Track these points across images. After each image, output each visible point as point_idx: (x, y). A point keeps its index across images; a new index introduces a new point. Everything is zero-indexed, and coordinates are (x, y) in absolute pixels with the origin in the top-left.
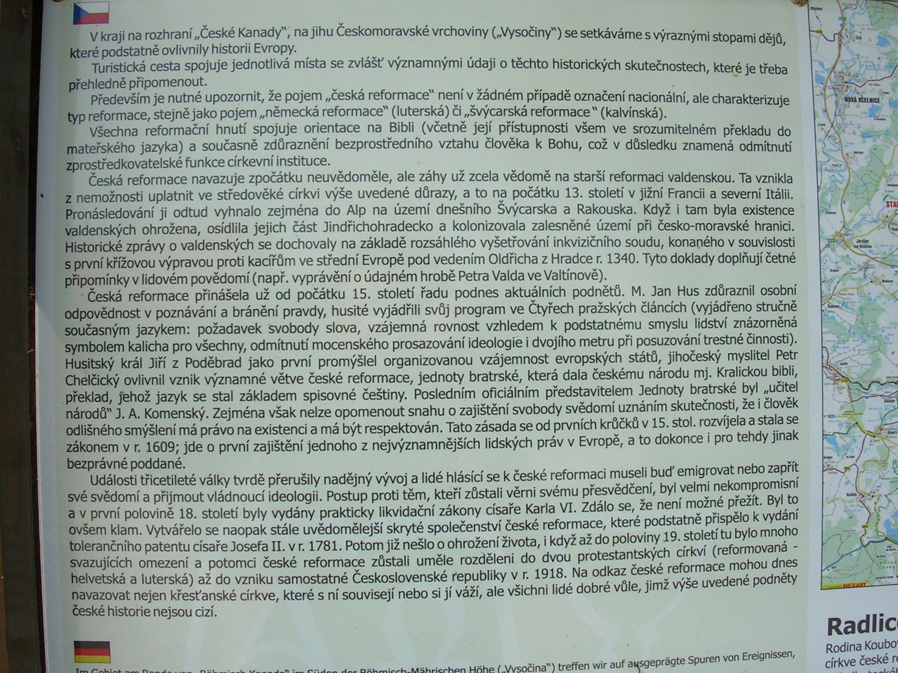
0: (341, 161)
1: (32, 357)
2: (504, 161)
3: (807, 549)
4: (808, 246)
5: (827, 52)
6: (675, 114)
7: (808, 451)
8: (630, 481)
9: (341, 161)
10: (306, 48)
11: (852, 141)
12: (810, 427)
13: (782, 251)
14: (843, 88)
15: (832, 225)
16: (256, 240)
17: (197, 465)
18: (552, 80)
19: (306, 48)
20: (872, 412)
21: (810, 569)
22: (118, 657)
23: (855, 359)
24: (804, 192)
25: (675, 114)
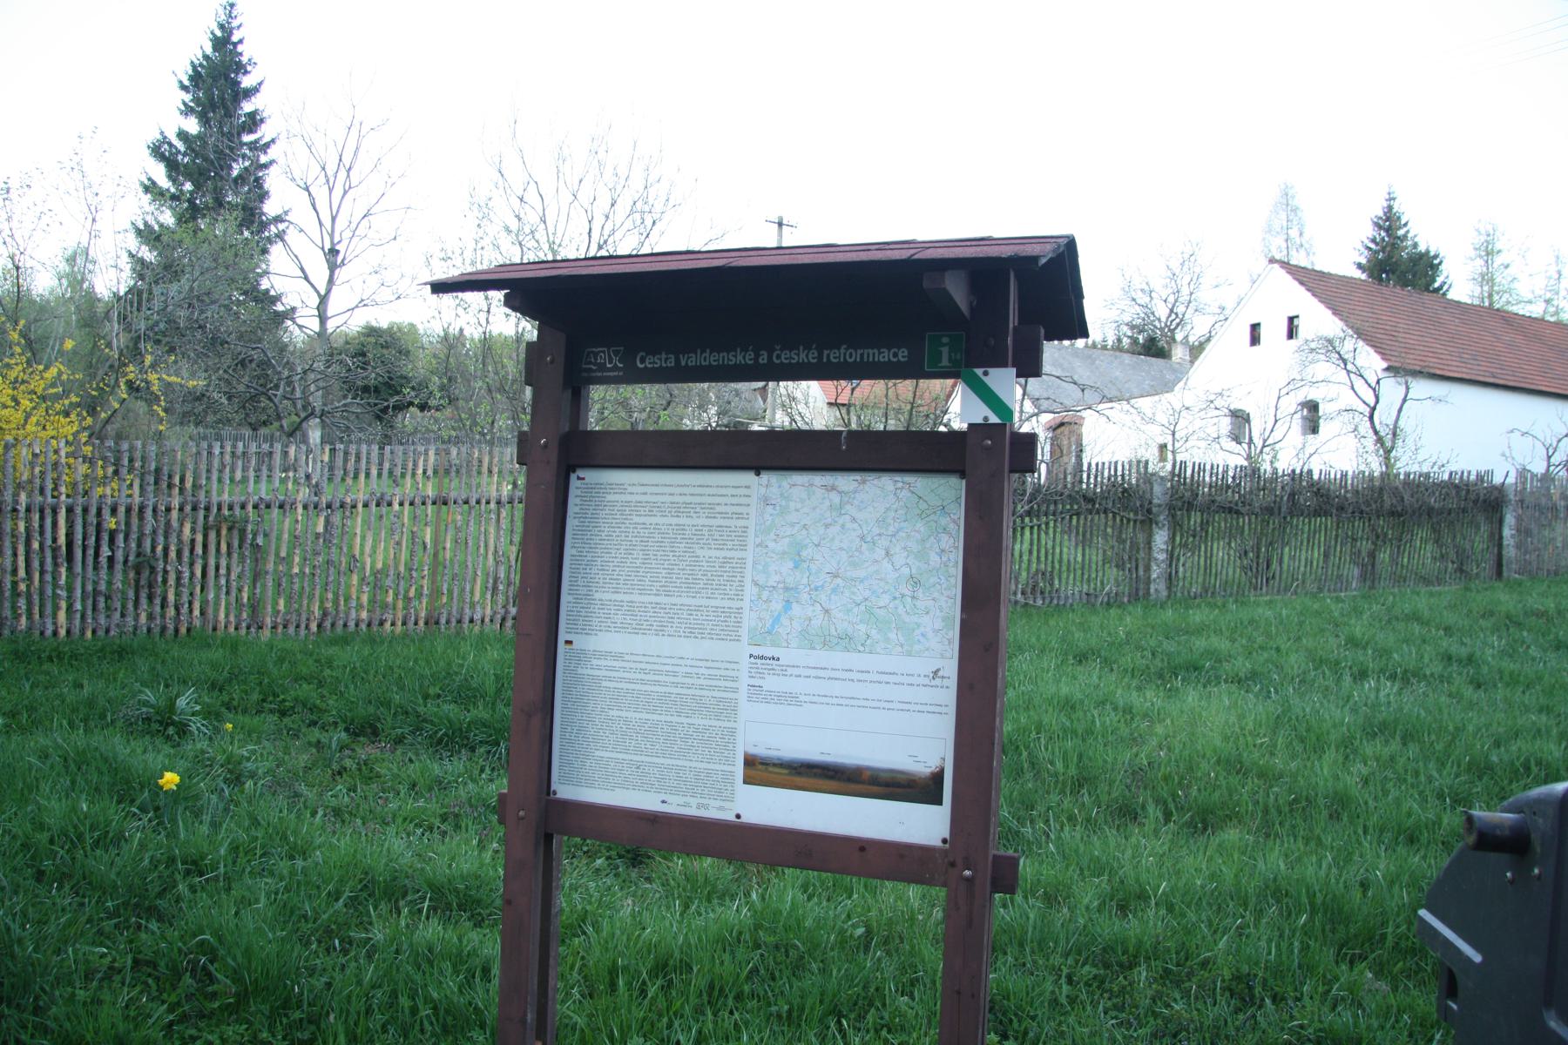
0: (637, 519)
1: (1302, 283)
2: (675, 521)
3: (744, 633)
4: (750, 547)
5: (763, 490)
6: (718, 509)
7: (746, 604)
8: (698, 608)
9: (637, 519)
10: (630, 489)
11: (767, 516)
12: (747, 598)
13: (743, 547)
14: (766, 501)
15: (758, 541)
16: (80, 500)
17: (597, 596)
18: (688, 499)
19: (630, 489)
20: (765, 594)
21: (745, 639)
22: (575, 646)
23: (761, 580)
24: (751, 532)
25: (718, 509)
